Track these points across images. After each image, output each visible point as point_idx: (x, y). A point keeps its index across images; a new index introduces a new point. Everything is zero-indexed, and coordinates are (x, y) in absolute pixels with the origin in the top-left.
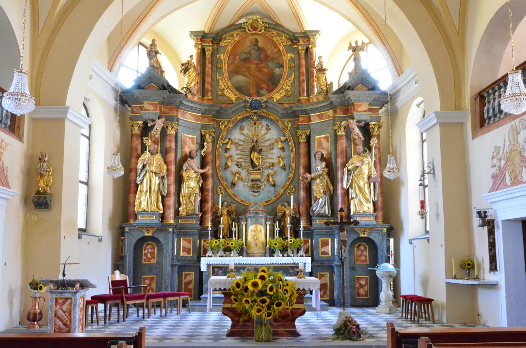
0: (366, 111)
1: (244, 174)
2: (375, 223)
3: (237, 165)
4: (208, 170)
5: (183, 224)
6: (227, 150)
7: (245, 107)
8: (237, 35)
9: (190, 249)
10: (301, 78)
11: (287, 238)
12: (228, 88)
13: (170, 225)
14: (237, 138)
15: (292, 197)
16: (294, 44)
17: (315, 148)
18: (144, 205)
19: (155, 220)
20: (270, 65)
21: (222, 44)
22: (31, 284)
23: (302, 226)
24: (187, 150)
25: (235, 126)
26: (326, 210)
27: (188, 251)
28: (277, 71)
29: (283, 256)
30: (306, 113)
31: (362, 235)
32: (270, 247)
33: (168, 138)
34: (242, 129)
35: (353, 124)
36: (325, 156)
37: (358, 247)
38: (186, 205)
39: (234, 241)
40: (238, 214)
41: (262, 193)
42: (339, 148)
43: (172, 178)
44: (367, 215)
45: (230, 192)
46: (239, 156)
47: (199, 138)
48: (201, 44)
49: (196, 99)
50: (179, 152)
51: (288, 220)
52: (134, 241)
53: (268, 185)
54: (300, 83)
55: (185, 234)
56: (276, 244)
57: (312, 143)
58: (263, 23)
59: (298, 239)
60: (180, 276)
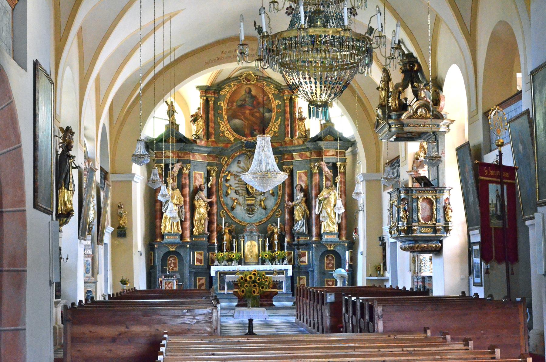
0: (333, 155)
1: (241, 199)
2: (338, 239)
3: (236, 192)
4: (214, 199)
5: (196, 242)
6: (227, 181)
7: (242, 146)
8: (234, 85)
9: (201, 260)
10: (286, 123)
11: (275, 251)
12: (228, 130)
13: (188, 243)
14: (235, 171)
15: (279, 219)
16: (281, 92)
17: (297, 182)
18: (168, 229)
19: (177, 239)
20: (261, 110)
21: (222, 93)
22: (121, 282)
23: (286, 241)
24: (197, 184)
25: (233, 162)
26: (304, 230)
27: (200, 261)
28: (267, 115)
29: (272, 264)
30: (290, 152)
31: (329, 249)
32: (262, 257)
33: (184, 176)
34: (239, 163)
35: (323, 165)
36: (303, 187)
37: (327, 257)
38: (198, 227)
39: (234, 254)
40: (238, 232)
41: (256, 215)
42: (314, 183)
43: (188, 207)
44: (332, 234)
45: (231, 215)
46: (237, 185)
47: (206, 173)
48: (205, 96)
49: (203, 142)
50: (192, 185)
51: (276, 236)
52: (162, 255)
53: (260, 209)
54: (286, 126)
55: (198, 249)
56: (266, 256)
57: (294, 176)
58: (255, 76)
59: (283, 252)
60: (195, 280)
